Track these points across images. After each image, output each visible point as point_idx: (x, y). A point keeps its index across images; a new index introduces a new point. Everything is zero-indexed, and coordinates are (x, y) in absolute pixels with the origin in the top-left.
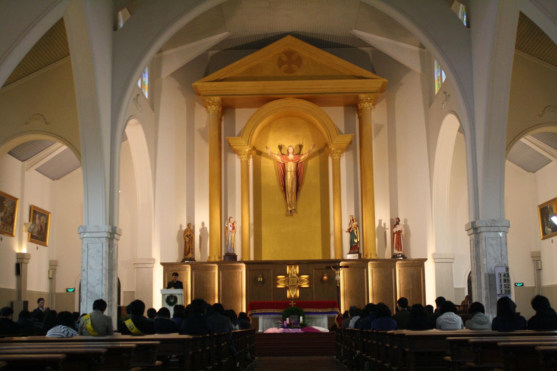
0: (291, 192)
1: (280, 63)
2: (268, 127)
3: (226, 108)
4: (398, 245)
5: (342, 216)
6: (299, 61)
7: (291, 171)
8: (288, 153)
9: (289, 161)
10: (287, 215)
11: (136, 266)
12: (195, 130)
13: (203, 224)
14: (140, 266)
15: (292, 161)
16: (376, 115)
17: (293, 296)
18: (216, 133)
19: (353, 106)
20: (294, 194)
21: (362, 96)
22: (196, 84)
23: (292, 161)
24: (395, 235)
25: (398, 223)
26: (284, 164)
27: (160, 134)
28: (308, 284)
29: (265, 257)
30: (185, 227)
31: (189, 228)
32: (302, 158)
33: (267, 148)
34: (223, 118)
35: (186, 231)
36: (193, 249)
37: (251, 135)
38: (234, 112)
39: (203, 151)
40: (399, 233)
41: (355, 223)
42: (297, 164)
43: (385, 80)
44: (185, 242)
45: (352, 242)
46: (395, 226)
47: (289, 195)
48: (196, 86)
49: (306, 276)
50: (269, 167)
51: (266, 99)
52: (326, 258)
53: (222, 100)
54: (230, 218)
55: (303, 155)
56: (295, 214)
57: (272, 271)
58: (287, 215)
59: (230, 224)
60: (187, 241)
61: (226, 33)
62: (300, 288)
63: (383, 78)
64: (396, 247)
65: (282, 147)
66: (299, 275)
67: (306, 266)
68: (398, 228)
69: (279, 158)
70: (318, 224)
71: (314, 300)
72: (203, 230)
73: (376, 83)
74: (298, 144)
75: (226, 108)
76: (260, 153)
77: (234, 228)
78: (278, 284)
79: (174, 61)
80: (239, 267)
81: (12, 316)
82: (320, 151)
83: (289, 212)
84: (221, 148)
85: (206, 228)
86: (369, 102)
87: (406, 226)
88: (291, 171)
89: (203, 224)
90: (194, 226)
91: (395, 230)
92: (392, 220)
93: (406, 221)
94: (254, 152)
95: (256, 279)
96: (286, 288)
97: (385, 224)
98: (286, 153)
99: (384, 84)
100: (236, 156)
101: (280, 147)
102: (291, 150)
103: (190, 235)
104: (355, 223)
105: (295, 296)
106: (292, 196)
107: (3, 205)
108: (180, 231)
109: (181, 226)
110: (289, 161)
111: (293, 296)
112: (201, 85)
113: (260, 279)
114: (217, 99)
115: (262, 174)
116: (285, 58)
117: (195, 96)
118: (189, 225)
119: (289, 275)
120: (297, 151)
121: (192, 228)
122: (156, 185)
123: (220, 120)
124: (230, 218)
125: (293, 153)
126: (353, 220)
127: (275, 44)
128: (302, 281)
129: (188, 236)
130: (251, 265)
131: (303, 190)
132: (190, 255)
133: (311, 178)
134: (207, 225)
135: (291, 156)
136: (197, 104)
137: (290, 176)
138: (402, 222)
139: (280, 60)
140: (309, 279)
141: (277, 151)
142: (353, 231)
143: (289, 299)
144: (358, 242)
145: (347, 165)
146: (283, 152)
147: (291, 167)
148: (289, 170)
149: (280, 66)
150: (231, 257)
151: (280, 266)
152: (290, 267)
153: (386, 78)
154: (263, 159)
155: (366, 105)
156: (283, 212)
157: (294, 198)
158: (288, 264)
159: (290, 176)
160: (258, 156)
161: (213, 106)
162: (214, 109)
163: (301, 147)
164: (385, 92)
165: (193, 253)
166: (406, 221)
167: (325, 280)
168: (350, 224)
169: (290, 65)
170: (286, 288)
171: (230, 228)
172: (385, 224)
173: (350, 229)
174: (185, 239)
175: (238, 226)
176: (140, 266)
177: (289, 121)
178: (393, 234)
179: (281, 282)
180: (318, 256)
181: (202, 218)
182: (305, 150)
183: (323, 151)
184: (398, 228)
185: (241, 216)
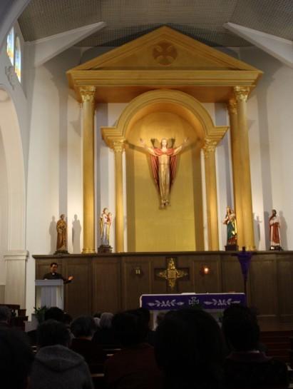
0: (165, 185)
1: (156, 54)
2: (141, 120)
3: (100, 103)
4: (276, 239)
5: (217, 211)
6: (174, 53)
7: (164, 164)
8: (162, 146)
9: (163, 153)
10: (160, 208)
11: (7, 258)
12: (69, 124)
13: (76, 216)
14: (11, 258)
15: (166, 153)
16: (248, 109)
18: (91, 123)
19: (226, 100)
20: (168, 187)
21: (238, 88)
22: (68, 72)
23: (166, 153)
24: (272, 227)
25: (274, 215)
27: (32, 124)
29: (139, 248)
30: (57, 219)
31: (62, 219)
32: (176, 151)
33: (141, 140)
34: (96, 112)
36: (66, 241)
37: (125, 126)
38: (107, 106)
39: (78, 143)
40: (276, 225)
41: (233, 215)
43: (261, 72)
44: (59, 234)
45: (229, 234)
46: (272, 218)
47: (162, 187)
48: (70, 75)
50: (142, 160)
51: (138, 91)
52: (200, 250)
53: (97, 90)
54: (105, 209)
55: (176, 148)
56: (168, 208)
57: (150, 264)
58: (160, 208)
59: (105, 215)
60: (60, 232)
61: (100, 23)
63: (260, 69)
64: (274, 239)
65: (156, 140)
68: (275, 221)
69: (152, 151)
70: (191, 218)
72: (76, 223)
73: (252, 74)
74: (170, 138)
75: (100, 103)
76: (133, 147)
77: (108, 220)
79: (49, 47)
81: (227, 244)
82: (192, 146)
83: (163, 206)
84: (99, 140)
85: (79, 221)
86: (244, 93)
87: (282, 218)
88: (164, 164)
89: (76, 216)
90: (66, 219)
91: (272, 222)
92: (266, 214)
93: (281, 213)
94: (127, 146)
95: (134, 271)
97: (258, 218)
98: (159, 146)
99: (260, 76)
100: (109, 149)
101: (153, 141)
102: (164, 143)
103: (63, 227)
104: (233, 215)
106: (165, 189)
107: (114, 319)
108: (52, 223)
109: (54, 218)
110: (163, 153)
112: (76, 73)
113: (138, 272)
114: (92, 88)
115: (135, 168)
116: (160, 49)
117: (71, 89)
118: (62, 217)
120: (170, 145)
121: (65, 220)
122: (29, 172)
123: (94, 114)
124: (105, 209)
125: (167, 146)
126: (230, 212)
127: (151, 34)
129: (60, 229)
131: (176, 182)
132: (63, 248)
133: (184, 172)
134: (81, 218)
135: (164, 149)
136: (69, 96)
137: (164, 169)
138: (277, 214)
139: (155, 50)
141: (150, 144)
142: (230, 223)
144: (236, 234)
146: (156, 145)
147: (164, 160)
148: (162, 162)
149: (156, 58)
153: (262, 70)
154: (136, 153)
155: (242, 97)
156: (156, 204)
157: (168, 191)
159: (164, 169)
160: (131, 150)
161: (88, 96)
162: (87, 99)
163: (173, 141)
164: (257, 87)
165: (66, 246)
166: (281, 213)
168: (227, 216)
169: (165, 55)
171: (105, 220)
172: (258, 218)
173: (227, 221)
174: (58, 231)
175: (112, 217)
176: (11, 258)
177: (165, 115)
178: (268, 226)
180: (191, 247)
181: (75, 211)
182: (176, 144)
183: (197, 145)
184: (275, 221)
185: (114, 204)
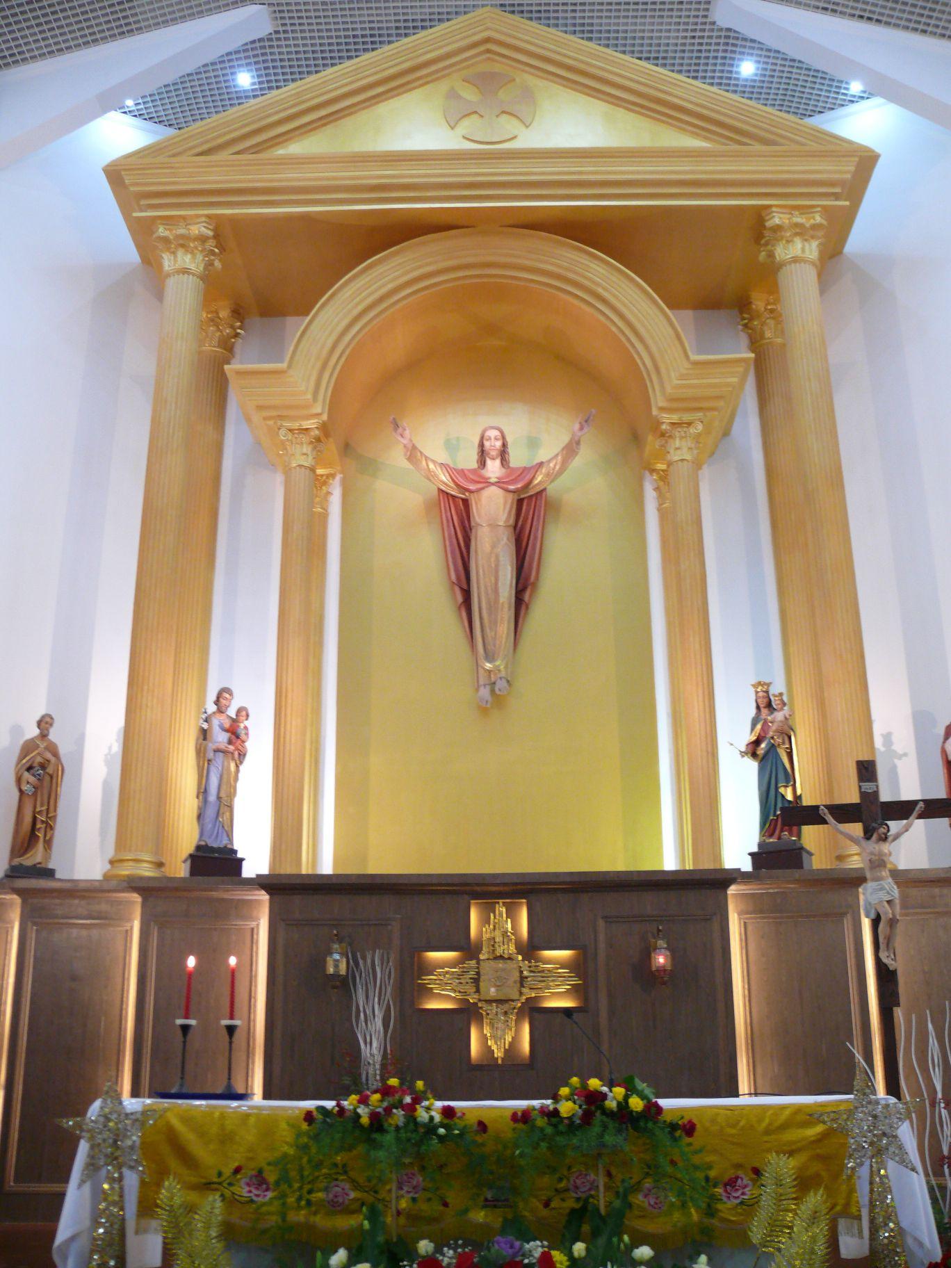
7: (493, 526)
17: (499, 1054)
26: (466, 502)
28: (575, 991)
35: (28, 747)
42: (520, 502)
49: (564, 954)
62: (533, 1011)
66: (530, 950)
67: (566, 900)
71: (304, 872)
78: (425, 991)
80: (244, 909)
96: (467, 1013)
105: (511, 1051)
110: (487, 483)
111: (499, 1054)
119: (479, 948)
128: (545, 976)
130: (297, 900)
132: (36, 856)
140: (579, 967)
142: (772, 748)
143: (479, 1067)
145: (251, 996)
150: (216, 862)
151: (418, 906)
152: (489, 909)
158: (476, 896)
167: (662, 970)
170: (467, 1013)
173: (757, 743)
179: (443, 985)
